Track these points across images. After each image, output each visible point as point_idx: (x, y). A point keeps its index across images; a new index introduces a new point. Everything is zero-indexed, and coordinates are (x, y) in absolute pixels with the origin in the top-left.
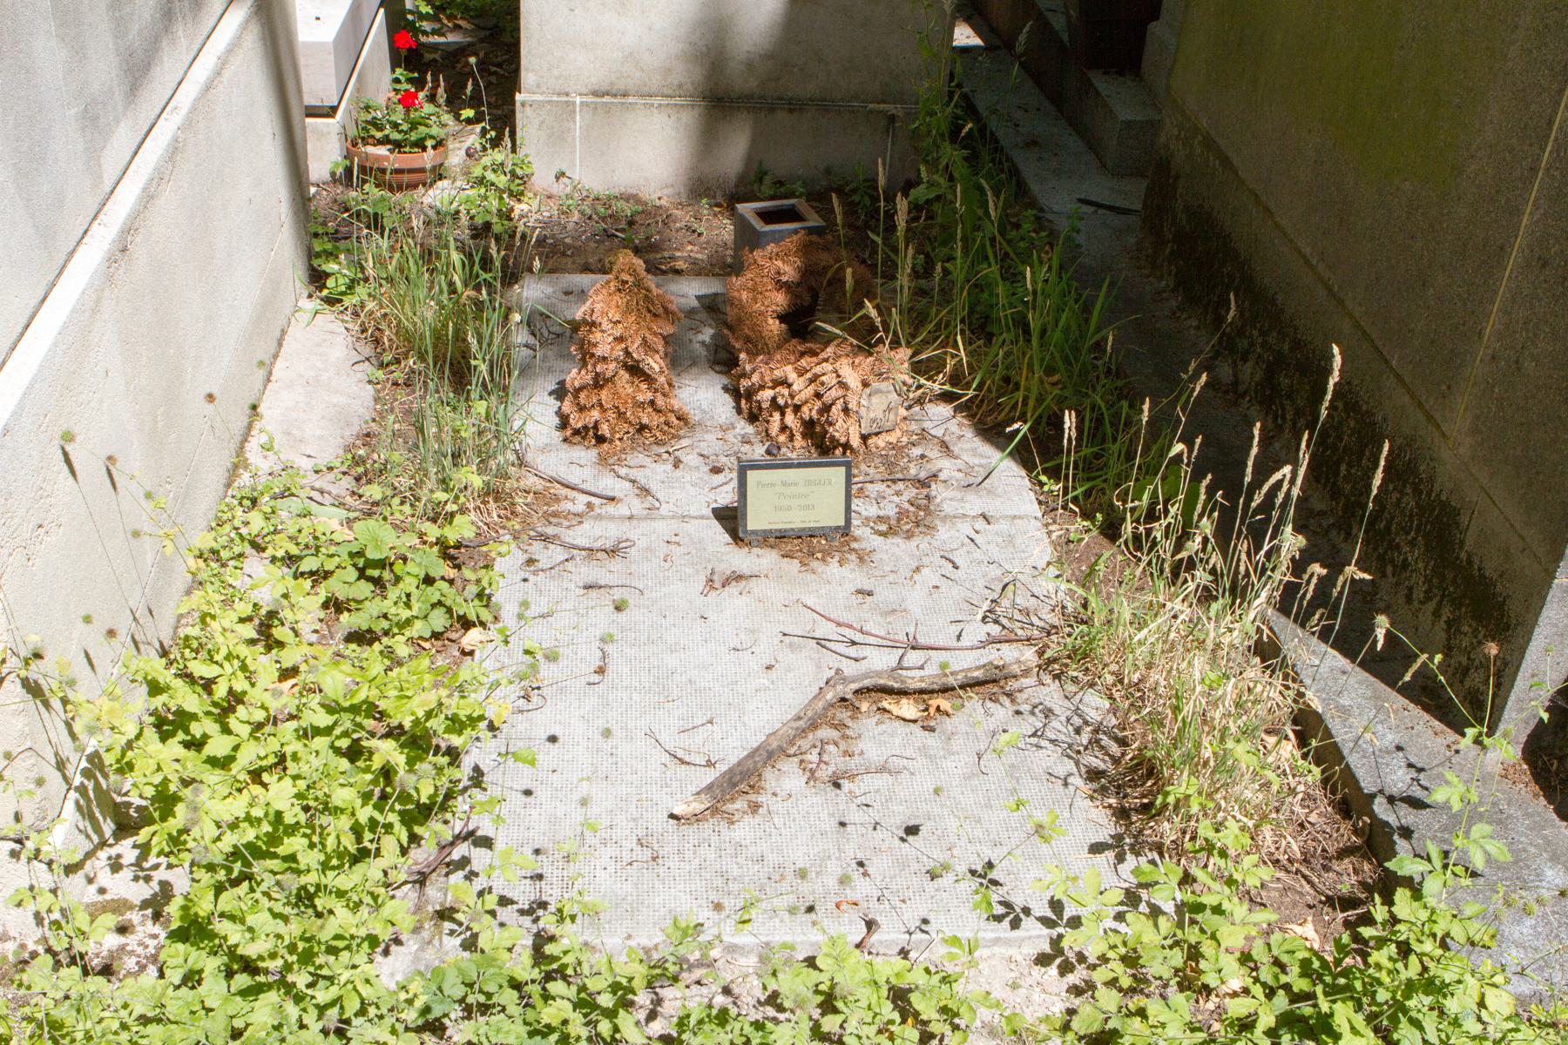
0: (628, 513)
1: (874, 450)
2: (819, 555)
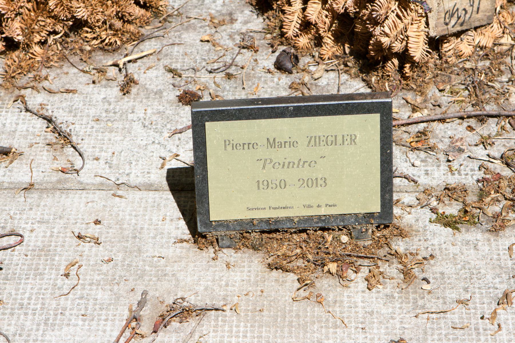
0: (26, 179)
1: (453, 60)
2: (333, 267)
